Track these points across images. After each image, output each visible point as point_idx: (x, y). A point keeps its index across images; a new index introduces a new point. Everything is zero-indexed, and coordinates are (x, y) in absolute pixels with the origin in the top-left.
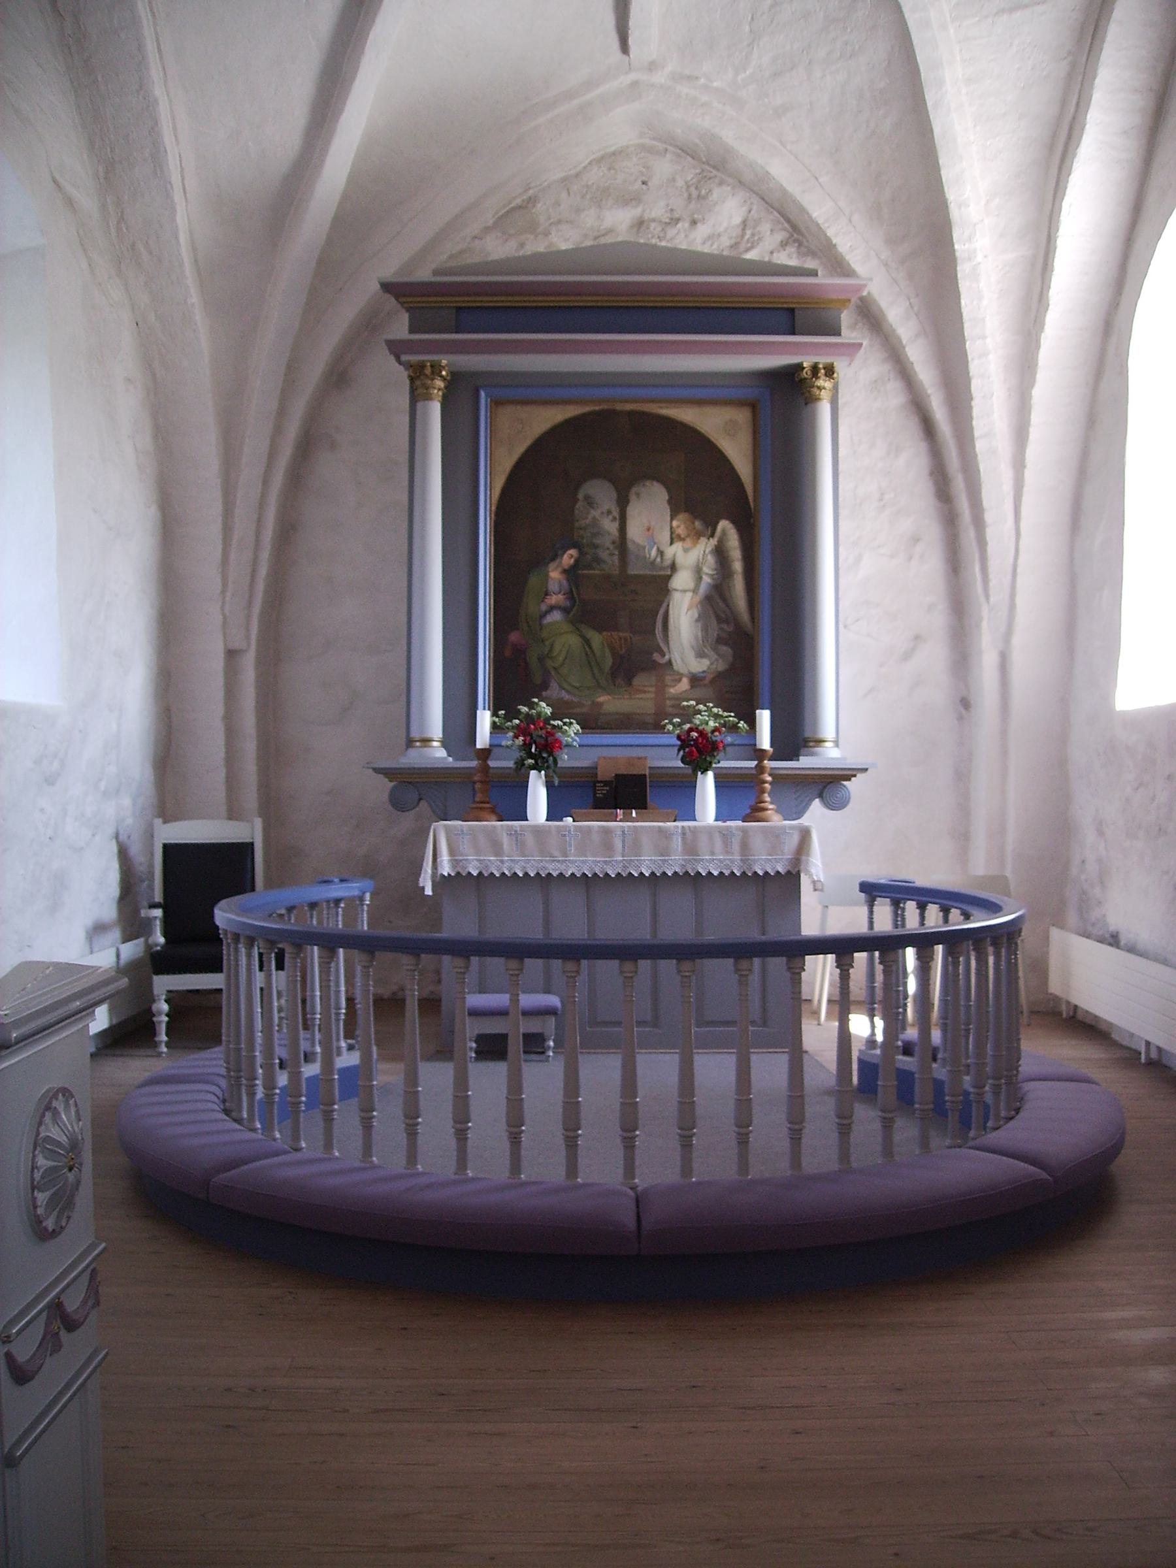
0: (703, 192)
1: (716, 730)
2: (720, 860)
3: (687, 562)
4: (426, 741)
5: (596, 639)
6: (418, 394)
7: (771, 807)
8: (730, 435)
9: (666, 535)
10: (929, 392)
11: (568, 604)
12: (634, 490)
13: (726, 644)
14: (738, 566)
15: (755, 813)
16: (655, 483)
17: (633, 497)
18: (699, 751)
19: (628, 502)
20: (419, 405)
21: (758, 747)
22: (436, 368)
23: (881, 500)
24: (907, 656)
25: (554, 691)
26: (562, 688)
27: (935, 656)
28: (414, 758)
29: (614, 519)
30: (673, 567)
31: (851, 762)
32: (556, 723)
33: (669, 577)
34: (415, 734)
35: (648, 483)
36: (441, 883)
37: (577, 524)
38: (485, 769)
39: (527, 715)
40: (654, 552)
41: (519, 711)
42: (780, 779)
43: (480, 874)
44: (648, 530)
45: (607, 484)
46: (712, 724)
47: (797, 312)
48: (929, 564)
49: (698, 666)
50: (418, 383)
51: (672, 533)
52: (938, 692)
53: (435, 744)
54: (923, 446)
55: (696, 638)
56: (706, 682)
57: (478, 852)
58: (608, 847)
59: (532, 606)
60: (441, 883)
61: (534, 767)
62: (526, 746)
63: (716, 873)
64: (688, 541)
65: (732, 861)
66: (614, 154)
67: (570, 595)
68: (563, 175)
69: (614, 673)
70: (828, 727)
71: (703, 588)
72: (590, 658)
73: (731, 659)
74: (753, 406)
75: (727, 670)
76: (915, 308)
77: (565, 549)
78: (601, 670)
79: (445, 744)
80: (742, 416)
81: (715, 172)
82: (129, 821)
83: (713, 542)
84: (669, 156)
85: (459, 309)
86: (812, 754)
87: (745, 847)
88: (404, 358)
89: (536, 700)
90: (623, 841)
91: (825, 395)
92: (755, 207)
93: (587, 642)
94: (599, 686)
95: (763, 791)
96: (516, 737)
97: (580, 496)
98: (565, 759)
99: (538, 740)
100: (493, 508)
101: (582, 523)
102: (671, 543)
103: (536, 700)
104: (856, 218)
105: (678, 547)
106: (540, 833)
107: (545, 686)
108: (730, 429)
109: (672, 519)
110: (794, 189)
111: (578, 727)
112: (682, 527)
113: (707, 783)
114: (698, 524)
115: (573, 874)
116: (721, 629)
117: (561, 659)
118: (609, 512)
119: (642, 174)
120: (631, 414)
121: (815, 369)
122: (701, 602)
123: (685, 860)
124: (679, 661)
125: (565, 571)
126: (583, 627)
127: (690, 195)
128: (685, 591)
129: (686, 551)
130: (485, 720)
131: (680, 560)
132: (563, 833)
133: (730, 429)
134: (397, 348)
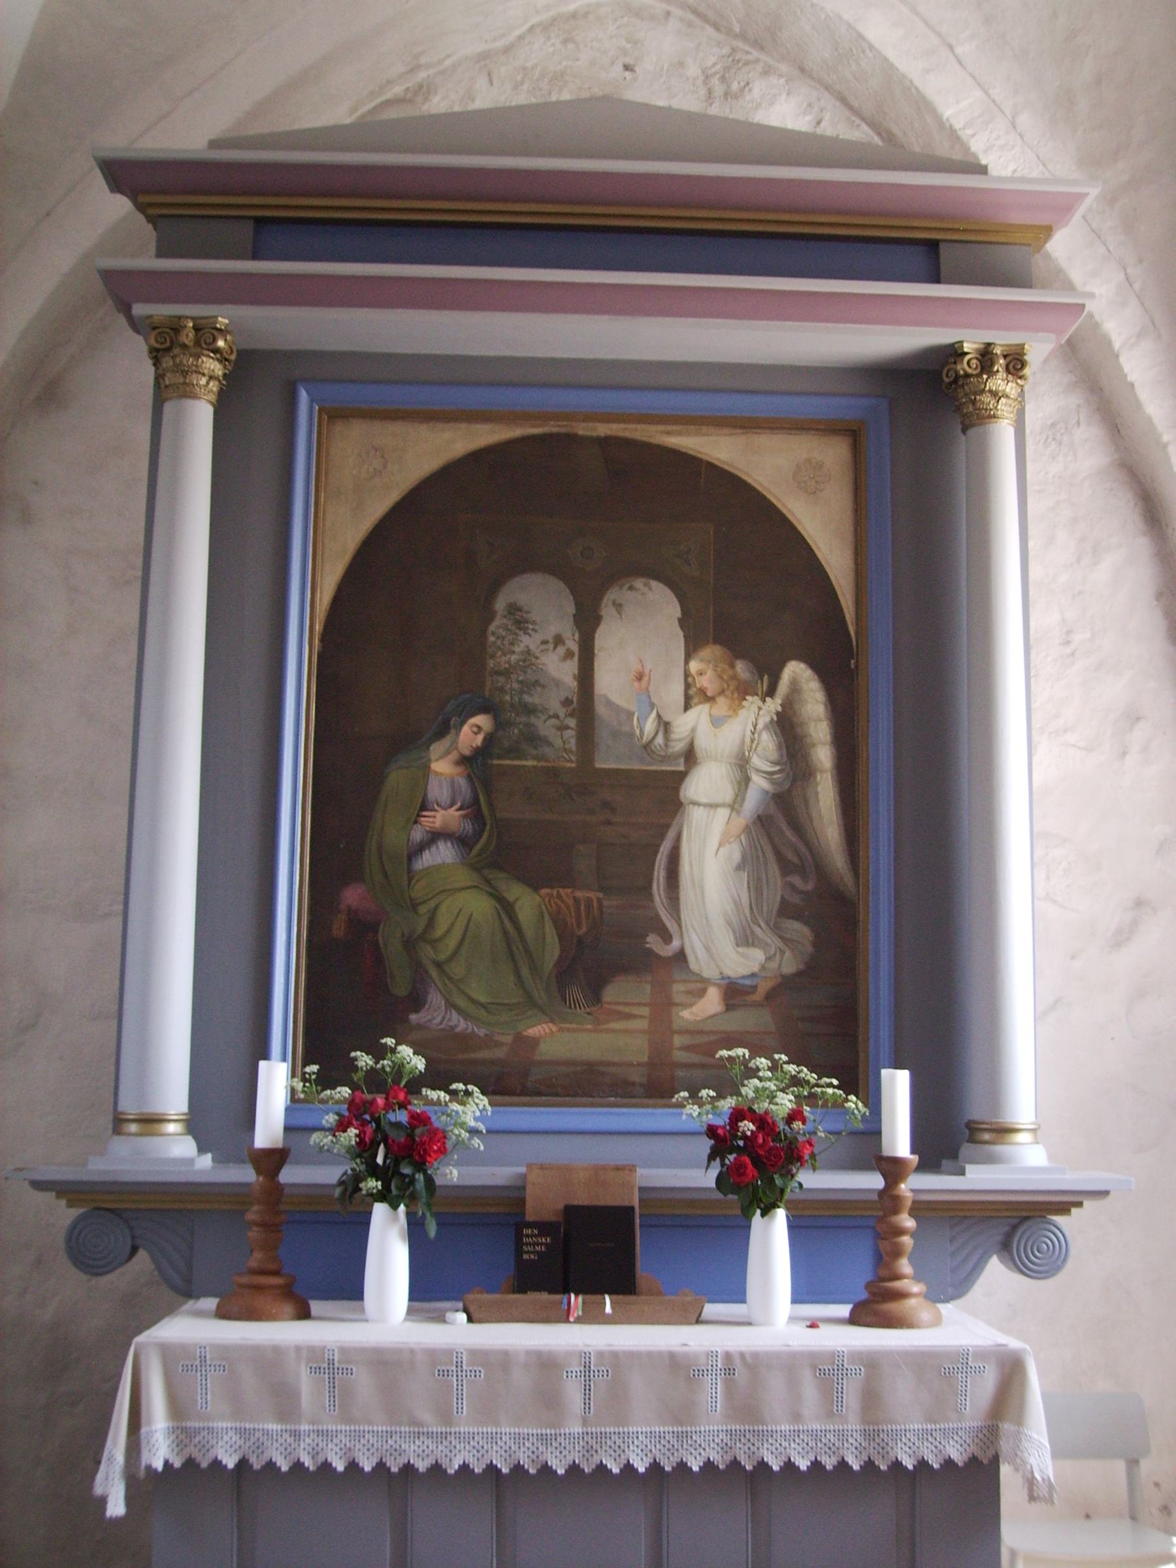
0: (735, 86)
1: (795, 1116)
2: (814, 1434)
3: (720, 745)
4: (151, 1122)
5: (528, 904)
6: (168, 389)
7: (916, 1288)
8: (809, 493)
9: (677, 691)
10: (1166, 438)
11: (468, 827)
12: (611, 595)
13: (798, 916)
14: (823, 755)
16: (654, 584)
17: (607, 611)
18: (756, 1163)
19: (597, 620)
20: (168, 407)
21: (887, 1152)
22: (205, 333)
23: (1068, 643)
24: (1121, 939)
25: (435, 1014)
26: (451, 1005)
29: (569, 655)
30: (690, 756)
32: (433, 1095)
33: (681, 776)
34: (128, 1105)
35: (639, 583)
36: (145, 1486)
37: (491, 663)
38: (274, 1193)
39: (372, 1073)
40: (650, 725)
41: (352, 1065)
42: (923, 1209)
43: (243, 1463)
44: (640, 677)
45: (556, 585)
46: (786, 1102)
47: (944, 250)
49: (741, 962)
50: (167, 362)
51: (688, 686)
53: (172, 1128)
55: (737, 904)
56: (758, 996)
57: (238, 1410)
58: (548, 1400)
59: (392, 831)
60: (145, 1486)
61: (382, 1196)
62: (365, 1149)
63: (803, 1464)
64: (722, 701)
65: (842, 1435)
66: (574, 16)
67: (473, 810)
68: (481, 47)
69: (564, 974)
71: (752, 801)
72: (513, 943)
73: (809, 949)
74: (854, 434)
75: (800, 974)
76: (1137, 286)
77: (466, 713)
78: (534, 968)
79: (194, 1124)
80: (833, 454)
81: (755, 54)
83: (773, 705)
84: (673, 24)
85: (259, 221)
86: (991, 1159)
88: (139, 310)
89: (390, 1041)
90: (587, 1389)
91: (1004, 408)
92: (827, 116)
93: (507, 908)
94: (531, 1002)
95: (897, 1253)
96: (342, 1126)
97: (500, 605)
98: (450, 1173)
99: (392, 1134)
100: (318, 627)
101: (503, 661)
102: (687, 708)
103: (390, 1041)
104: (1024, 120)
105: (700, 714)
107: (416, 1001)
108: (808, 479)
109: (687, 662)
110: (909, 66)
111: (484, 1101)
112: (710, 673)
113: (773, 1236)
114: (742, 669)
115: (465, 1467)
116: (793, 888)
117: (452, 942)
118: (559, 640)
119: (625, 52)
120: (606, 442)
121: (986, 356)
122: (747, 829)
123: (729, 1432)
124: (701, 953)
125: (464, 761)
126: (491, 874)
127: (710, 91)
128: (713, 806)
129: (716, 722)
130: (276, 1082)
131: (704, 743)
133: (808, 479)
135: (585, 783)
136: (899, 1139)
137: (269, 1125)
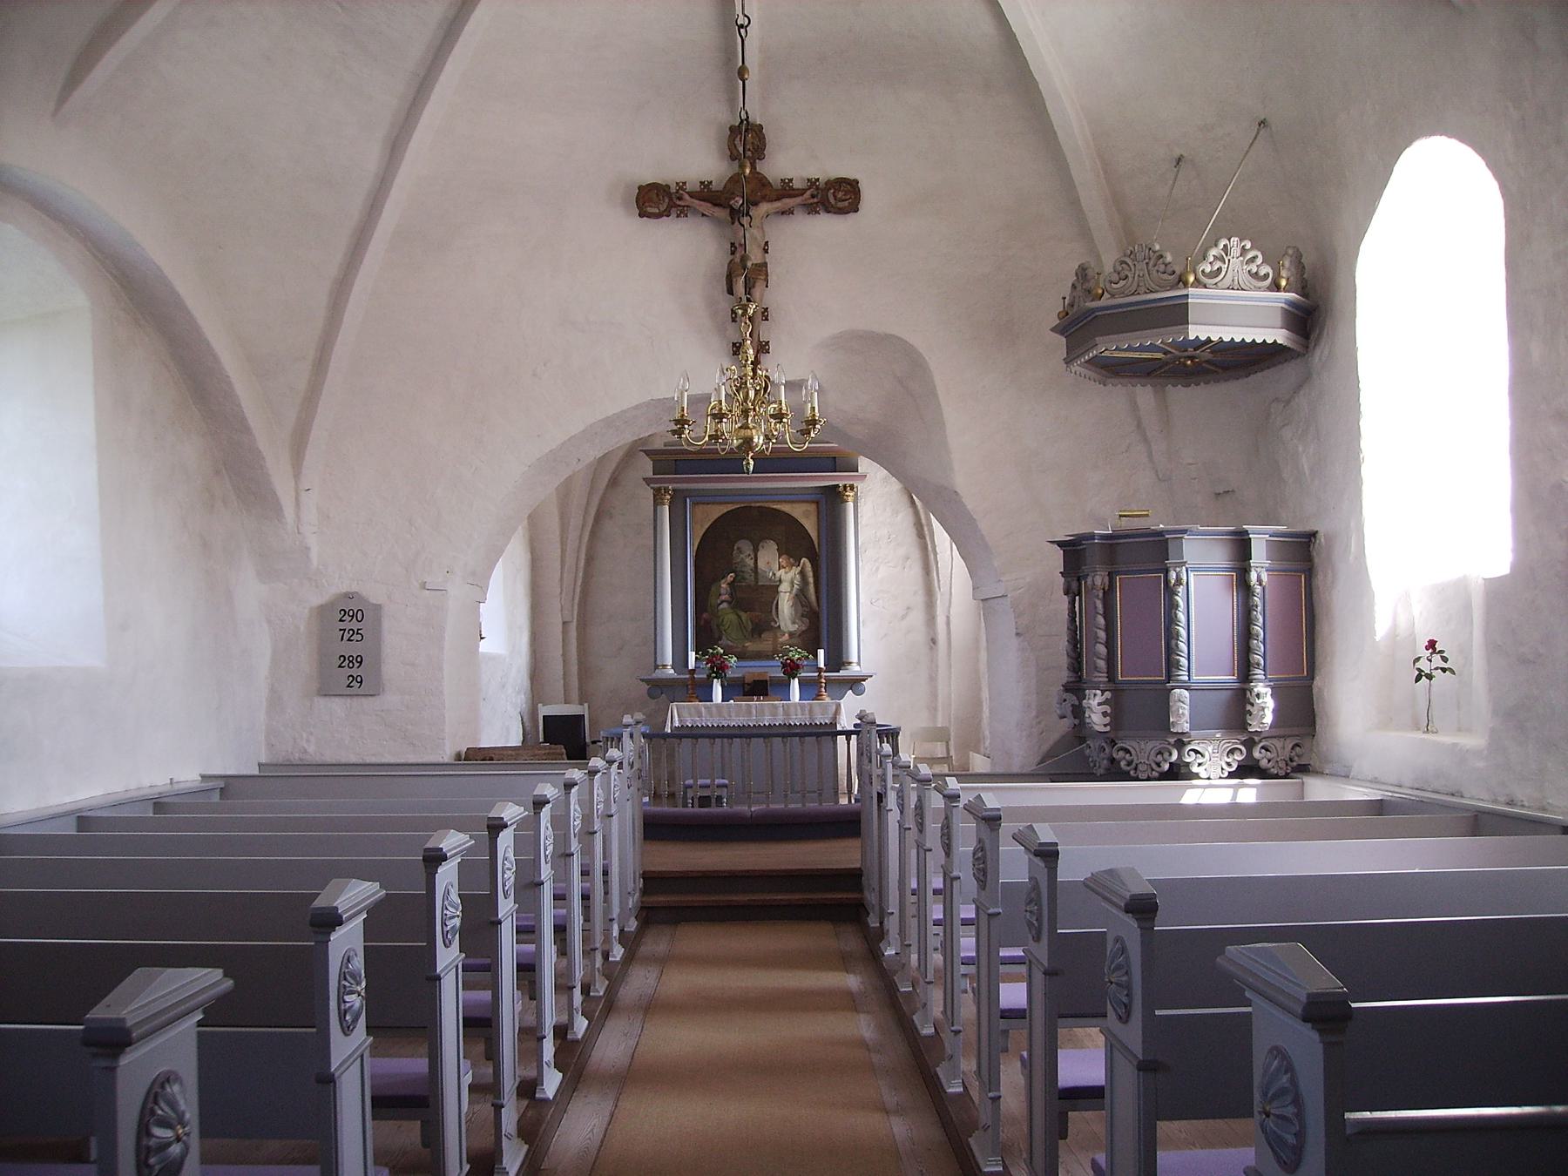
3: (787, 578)
4: (665, 666)
5: (744, 616)
14: (811, 580)
15: (818, 696)
18: (791, 669)
22: (667, 490)
24: (903, 617)
25: (724, 641)
27: (917, 617)
28: (658, 674)
31: (865, 672)
48: (915, 570)
49: (793, 628)
52: (920, 636)
54: (910, 510)
58: (750, 713)
59: (713, 601)
69: (753, 630)
70: (854, 657)
80: (813, 507)
82: (1417, 609)
87: (811, 711)
98: (729, 674)
106: (719, 708)
108: (806, 514)
113: (795, 684)
130: (692, 656)
132: (729, 707)
133: (806, 514)
134: (648, 481)
135: (757, 588)
136: (822, 665)
137: (692, 664)
